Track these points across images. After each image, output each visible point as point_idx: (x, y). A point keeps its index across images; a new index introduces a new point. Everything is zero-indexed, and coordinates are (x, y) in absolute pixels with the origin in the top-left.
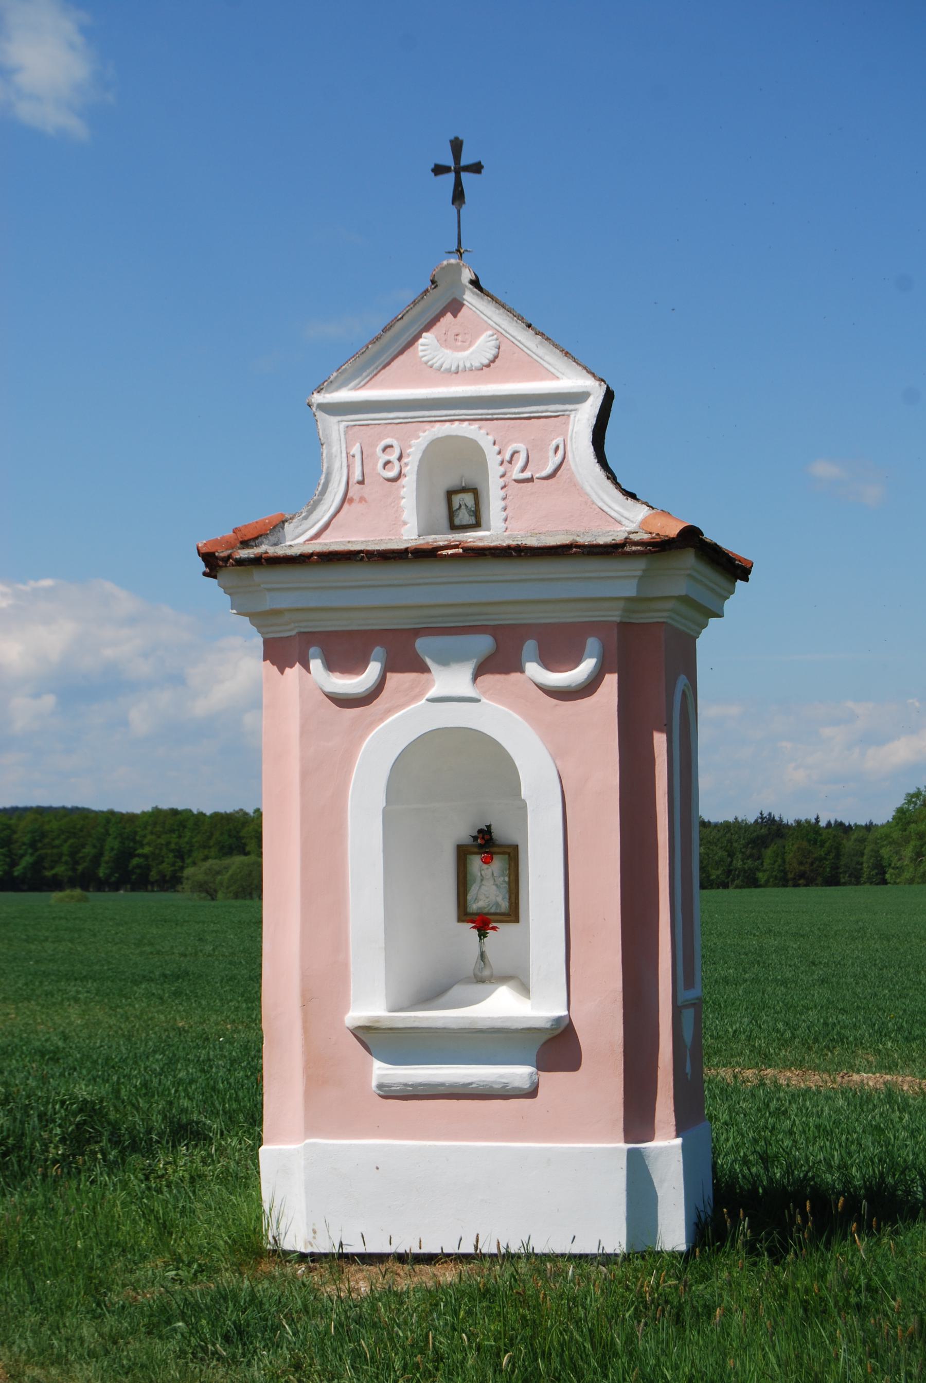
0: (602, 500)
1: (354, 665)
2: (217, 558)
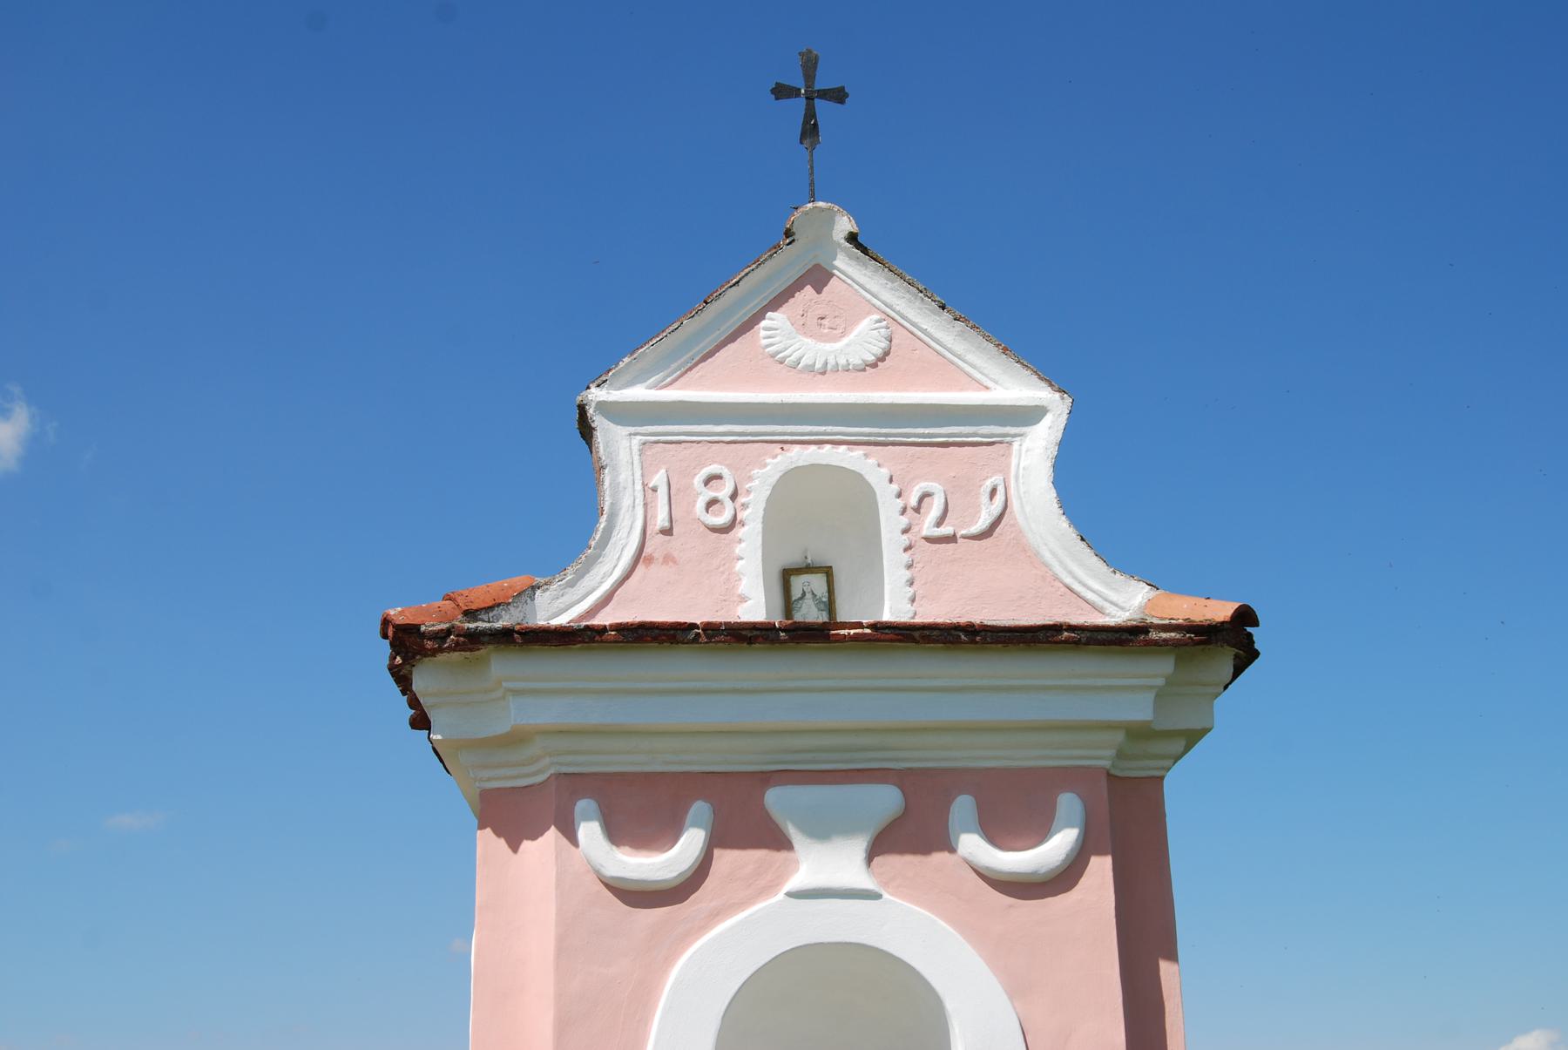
0: (1070, 573)
1: (660, 833)
2: (423, 635)
